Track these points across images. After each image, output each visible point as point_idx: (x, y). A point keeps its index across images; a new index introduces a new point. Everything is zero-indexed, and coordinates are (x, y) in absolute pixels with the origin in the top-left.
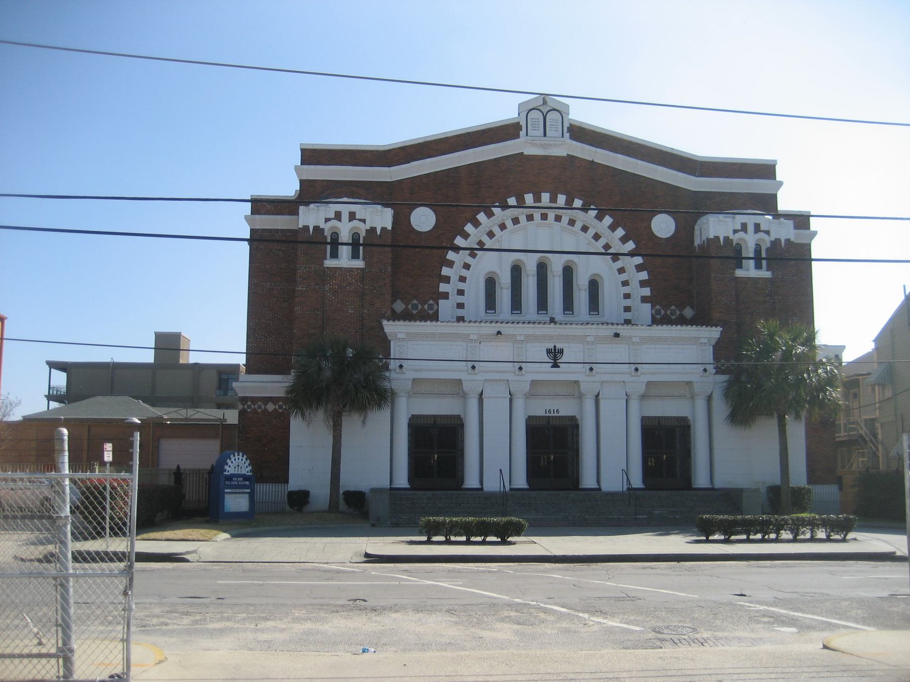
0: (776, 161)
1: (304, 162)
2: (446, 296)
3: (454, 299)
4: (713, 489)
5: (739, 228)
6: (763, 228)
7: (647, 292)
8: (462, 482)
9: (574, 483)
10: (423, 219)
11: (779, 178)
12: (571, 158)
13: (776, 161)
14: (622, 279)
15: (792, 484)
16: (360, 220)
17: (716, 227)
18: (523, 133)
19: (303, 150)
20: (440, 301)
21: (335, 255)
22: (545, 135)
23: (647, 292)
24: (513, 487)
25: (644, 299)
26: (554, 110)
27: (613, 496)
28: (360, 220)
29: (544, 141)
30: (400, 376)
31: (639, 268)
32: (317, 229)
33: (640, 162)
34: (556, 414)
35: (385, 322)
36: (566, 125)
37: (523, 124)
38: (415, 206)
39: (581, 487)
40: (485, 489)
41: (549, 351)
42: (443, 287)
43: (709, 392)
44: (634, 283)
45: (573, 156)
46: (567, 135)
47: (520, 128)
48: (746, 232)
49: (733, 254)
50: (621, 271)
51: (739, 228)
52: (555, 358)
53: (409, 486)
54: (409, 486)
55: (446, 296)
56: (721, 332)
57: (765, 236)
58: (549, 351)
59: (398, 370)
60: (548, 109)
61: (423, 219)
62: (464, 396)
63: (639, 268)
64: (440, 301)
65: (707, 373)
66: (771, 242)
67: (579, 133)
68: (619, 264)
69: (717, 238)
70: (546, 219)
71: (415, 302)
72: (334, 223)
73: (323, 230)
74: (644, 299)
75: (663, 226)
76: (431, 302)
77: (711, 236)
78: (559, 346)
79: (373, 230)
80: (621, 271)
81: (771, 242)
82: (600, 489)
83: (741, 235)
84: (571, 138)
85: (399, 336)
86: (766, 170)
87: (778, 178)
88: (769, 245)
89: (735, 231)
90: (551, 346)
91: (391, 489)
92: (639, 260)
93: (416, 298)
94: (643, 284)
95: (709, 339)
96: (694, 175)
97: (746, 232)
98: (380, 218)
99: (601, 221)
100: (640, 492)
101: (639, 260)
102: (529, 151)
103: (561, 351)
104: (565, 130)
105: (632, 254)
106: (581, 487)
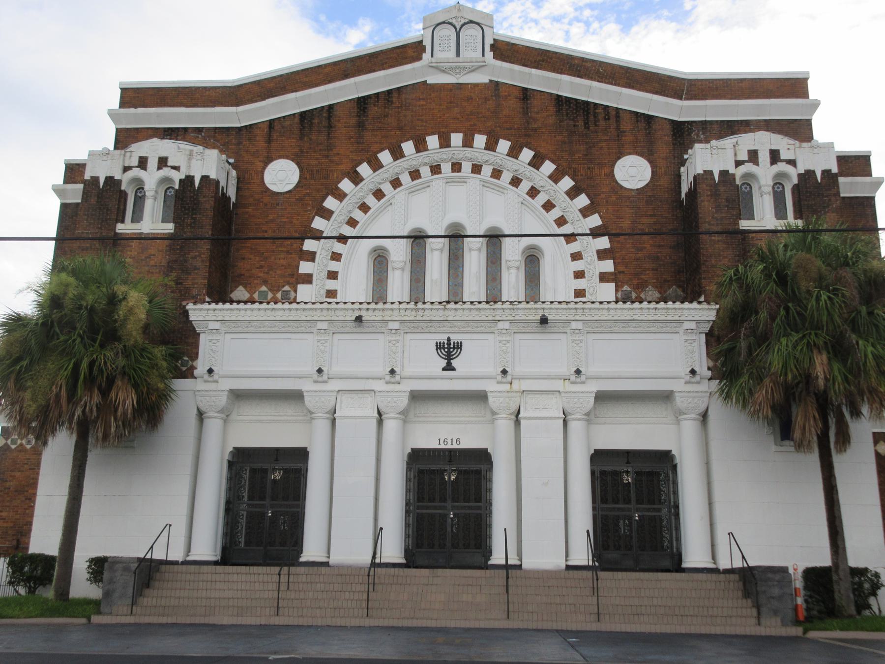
0: (808, 73)
1: (124, 104)
2: (308, 279)
3: (321, 284)
7: (608, 266)
8: (300, 551)
16: (173, 168)
17: (706, 159)
18: (426, 56)
19: (124, 90)
20: (299, 286)
21: (137, 217)
23: (608, 266)
24: (570, 563)
25: (604, 277)
26: (471, 22)
28: (173, 168)
29: (457, 59)
30: (212, 386)
31: (602, 255)
34: (455, 446)
35: (190, 306)
36: (489, 41)
37: (427, 43)
38: (269, 160)
39: (684, 565)
41: (439, 346)
42: (305, 267)
44: (590, 255)
46: (489, 55)
48: (756, 163)
49: (732, 194)
50: (576, 256)
53: (403, 561)
54: (403, 561)
55: (308, 279)
56: (718, 311)
57: (789, 169)
58: (439, 346)
59: (206, 377)
60: (463, 21)
61: (281, 176)
63: (602, 255)
64: (299, 286)
65: (697, 378)
66: (799, 175)
67: (506, 51)
68: (575, 247)
69: (709, 173)
70: (459, 171)
71: (264, 288)
72: (136, 172)
73: (119, 182)
74: (604, 277)
76: (287, 288)
78: (455, 338)
79: (189, 179)
80: (576, 256)
81: (799, 175)
83: (748, 167)
85: (212, 325)
89: (738, 163)
90: (443, 338)
91: (569, 568)
92: (604, 243)
93: (265, 282)
94: (555, 177)
95: (698, 322)
97: (756, 163)
98: (207, 164)
100: (396, 571)
101: (604, 243)
102: (434, 79)
103: (459, 346)
104: (487, 48)
105: (595, 233)
106: (685, 565)
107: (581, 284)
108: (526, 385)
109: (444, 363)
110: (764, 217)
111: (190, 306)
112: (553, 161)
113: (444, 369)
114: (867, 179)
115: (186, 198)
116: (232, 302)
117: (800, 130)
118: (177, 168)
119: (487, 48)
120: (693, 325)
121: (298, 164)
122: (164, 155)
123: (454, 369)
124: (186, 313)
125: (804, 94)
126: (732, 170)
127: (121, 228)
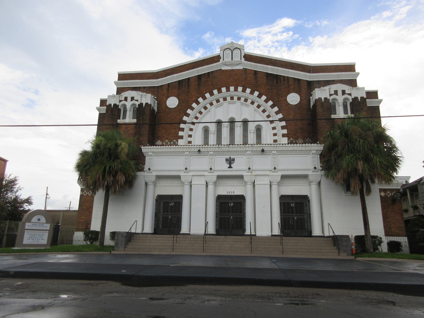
0: (355, 63)
1: (119, 79)
2: (182, 137)
4: (324, 237)
5: (333, 93)
6: (347, 92)
9: (309, 234)
10: (172, 102)
11: (357, 71)
12: (245, 70)
13: (355, 63)
14: (273, 131)
15: (372, 234)
16: (136, 100)
17: (319, 94)
18: (221, 60)
19: (119, 75)
20: (179, 140)
21: (124, 118)
22: (232, 59)
24: (273, 234)
25: (284, 136)
26: (237, 48)
27: (196, 237)
28: (136, 100)
30: (150, 174)
32: (115, 105)
33: (280, 68)
34: (233, 194)
35: (142, 147)
37: (221, 56)
38: (168, 97)
39: (313, 235)
40: (257, 235)
43: (319, 180)
45: (246, 69)
46: (243, 59)
47: (220, 58)
48: (337, 95)
50: (274, 128)
51: (333, 93)
52: (230, 164)
55: (182, 137)
58: (227, 160)
59: (148, 171)
61: (172, 102)
62: (183, 184)
63: (283, 127)
64: (179, 140)
65: (317, 170)
66: (352, 99)
67: (249, 58)
68: (273, 125)
69: (320, 99)
71: (167, 141)
73: (118, 105)
74: (284, 136)
75: (293, 99)
76: (175, 141)
77: (317, 98)
78: (232, 157)
79: (141, 104)
80: (274, 128)
81: (352, 99)
82: (255, 235)
84: (349, 236)
85: (150, 154)
86: (350, 68)
87: (357, 71)
88: (351, 101)
89: (331, 95)
90: (228, 157)
92: (284, 123)
93: (167, 139)
95: (317, 150)
96: (310, 73)
97: (337, 95)
98: (147, 99)
99: (260, 98)
100: (151, 235)
101: (284, 123)
103: (234, 160)
104: (242, 57)
106: (313, 235)
107: (276, 138)
108: (257, 173)
109: (228, 166)
110: (340, 114)
111: (142, 147)
112: (265, 96)
113: (228, 168)
114: (377, 100)
115: (140, 110)
116: (156, 146)
117: (353, 83)
118: (137, 101)
119: (242, 57)
120: (315, 152)
121: (178, 98)
122: (133, 96)
123: (232, 168)
124: (141, 150)
125: (377, 98)
126: (328, 97)
127: (119, 121)
